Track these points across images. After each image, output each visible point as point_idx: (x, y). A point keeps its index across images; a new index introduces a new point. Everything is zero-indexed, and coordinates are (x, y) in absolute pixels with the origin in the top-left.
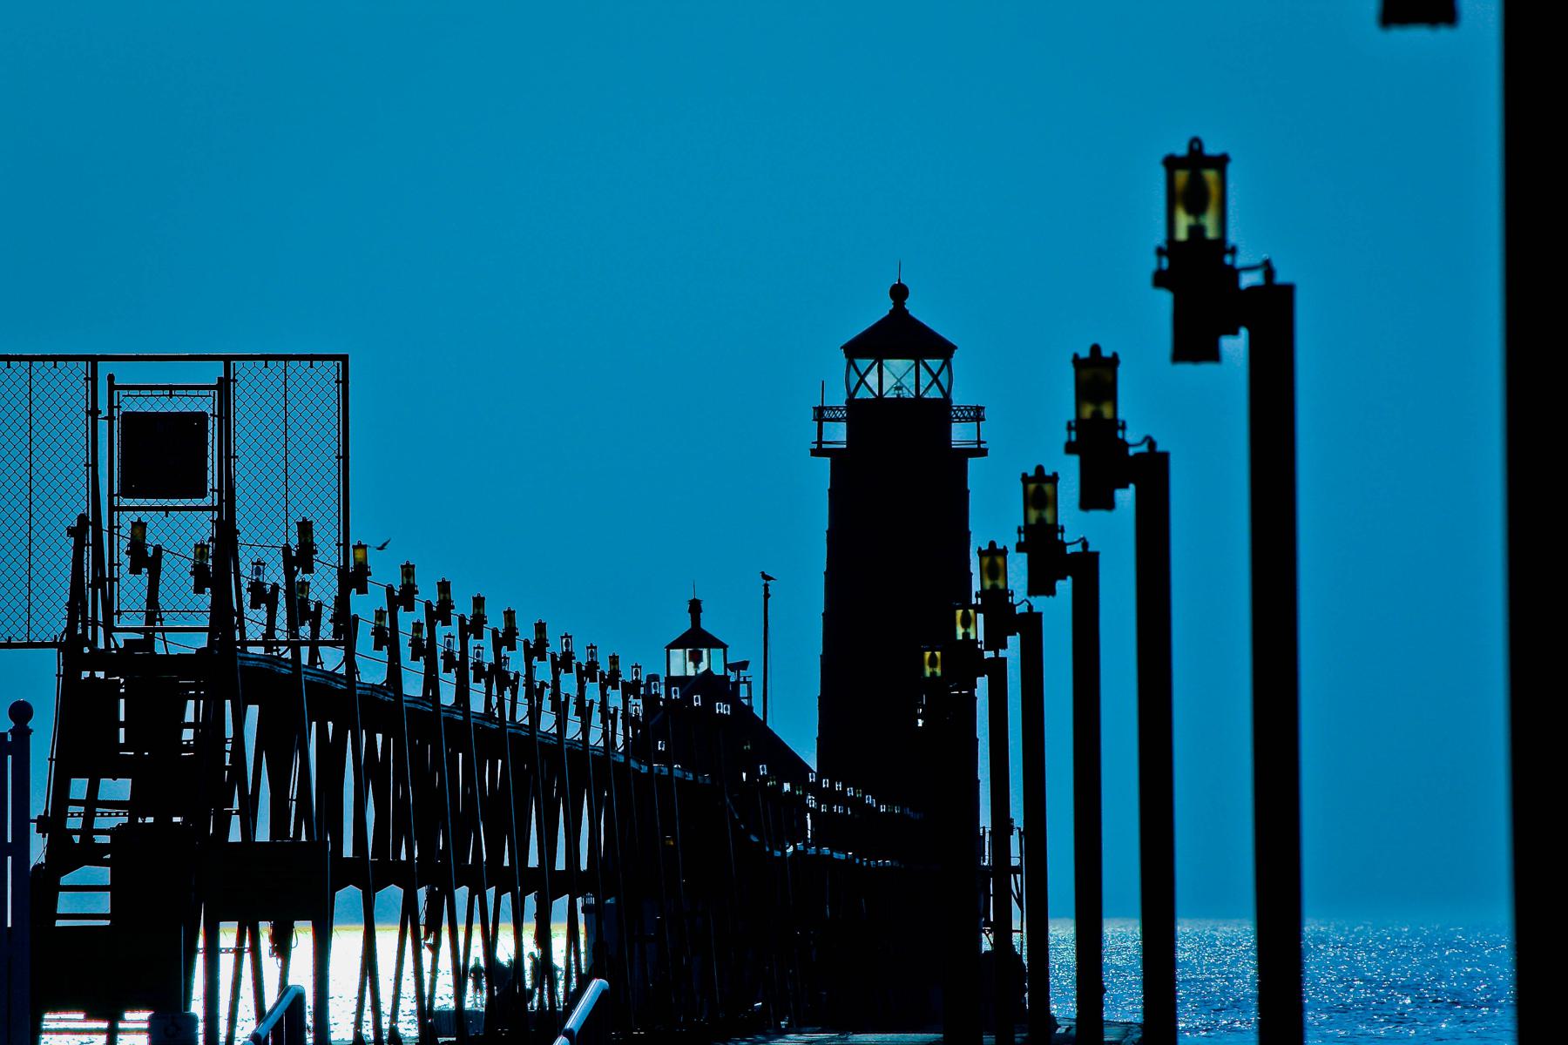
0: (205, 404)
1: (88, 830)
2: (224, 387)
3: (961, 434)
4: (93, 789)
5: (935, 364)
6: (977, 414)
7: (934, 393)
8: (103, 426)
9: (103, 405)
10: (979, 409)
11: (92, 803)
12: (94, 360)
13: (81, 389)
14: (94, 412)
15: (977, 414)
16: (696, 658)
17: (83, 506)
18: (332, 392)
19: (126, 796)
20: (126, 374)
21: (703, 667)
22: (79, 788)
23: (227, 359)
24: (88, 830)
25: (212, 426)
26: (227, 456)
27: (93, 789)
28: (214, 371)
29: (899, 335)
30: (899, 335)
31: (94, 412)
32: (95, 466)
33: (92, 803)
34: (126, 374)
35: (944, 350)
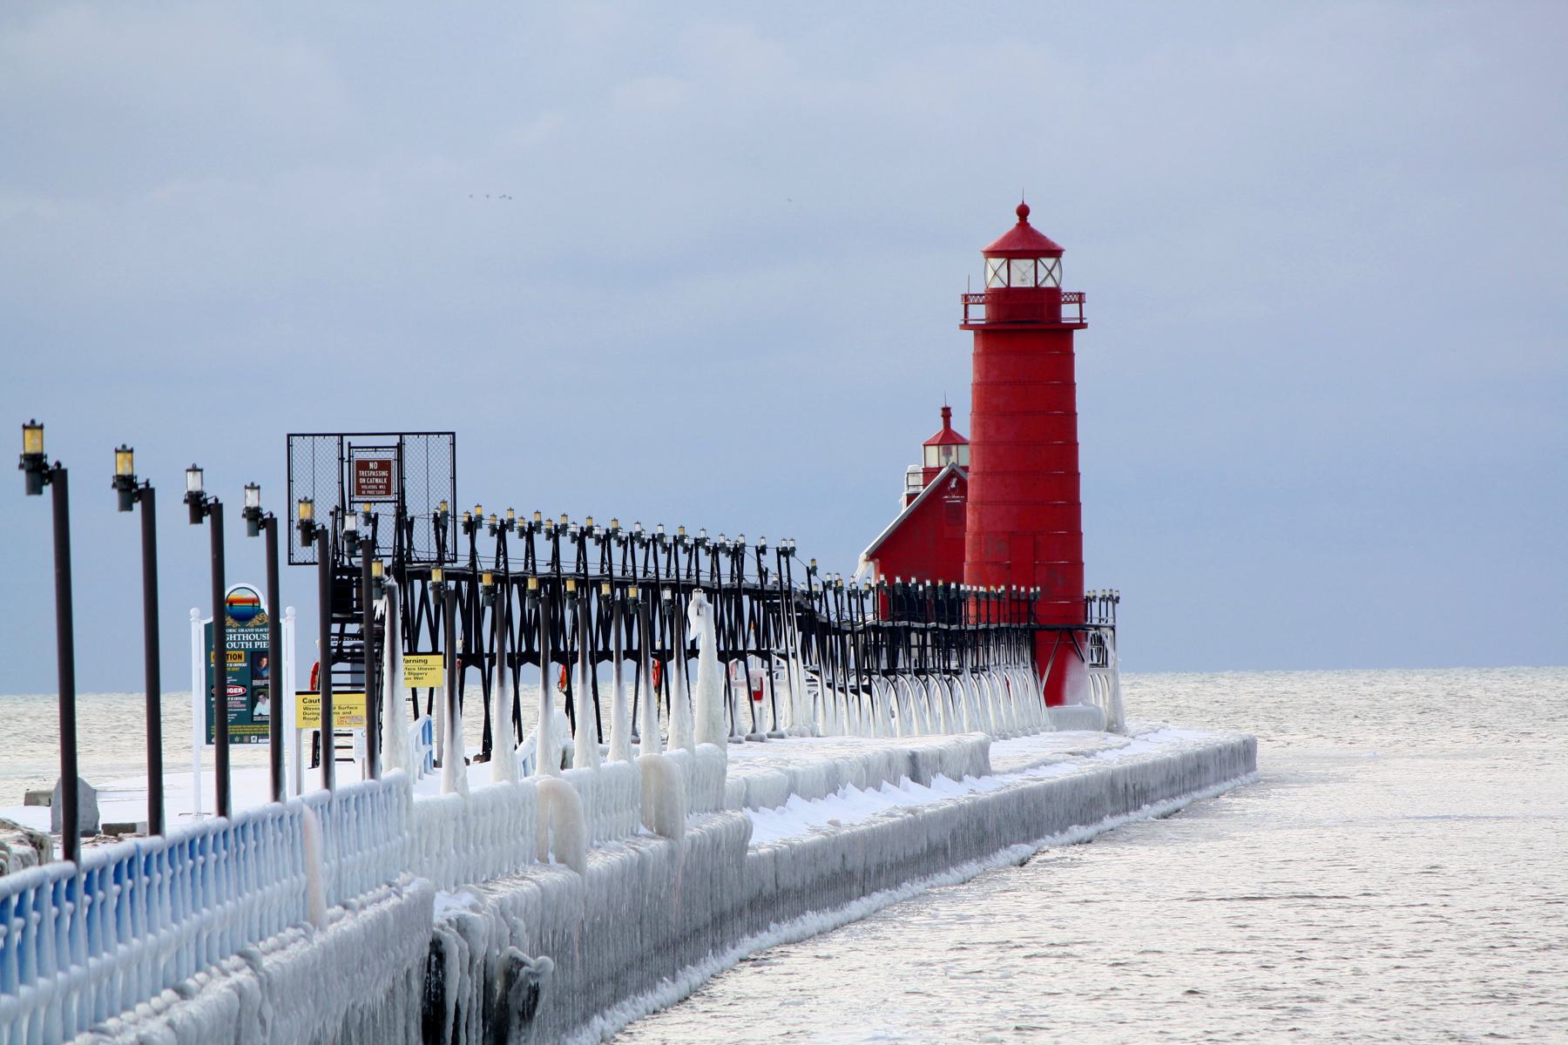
0: (391, 455)
1: (340, 647)
2: (400, 447)
3: (1068, 312)
4: (342, 629)
5: (1049, 262)
6: (1080, 298)
7: (1050, 284)
8: (346, 465)
9: (346, 456)
10: (1080, 295)
11: (342, 635)
12: (341, 435)
13: (336, 448)
14: (342, 459)
15: (1080, 298)
16: (948, 453)
17: (337, 502)
18: (448, 449)
19: (1064, 307)
20: (356, 441)
21: (953, 459)
22: (336, 628)
23: (401, 434)
24: (340, 647)
25: (394, 466)
26: (401, 478)
27: (342, 629)
28: (396, 439)
29: (1026, 243)
30: (1026, 243)
31: (342, 459)
32: (342, 483)
33: (342, 635)
34: (356, 441)
35: (1056, 253)
